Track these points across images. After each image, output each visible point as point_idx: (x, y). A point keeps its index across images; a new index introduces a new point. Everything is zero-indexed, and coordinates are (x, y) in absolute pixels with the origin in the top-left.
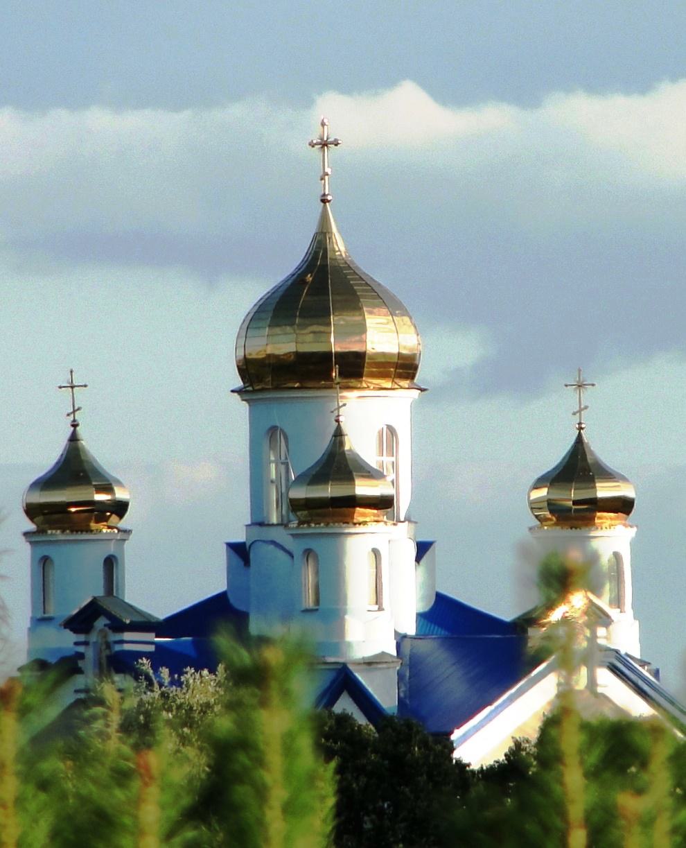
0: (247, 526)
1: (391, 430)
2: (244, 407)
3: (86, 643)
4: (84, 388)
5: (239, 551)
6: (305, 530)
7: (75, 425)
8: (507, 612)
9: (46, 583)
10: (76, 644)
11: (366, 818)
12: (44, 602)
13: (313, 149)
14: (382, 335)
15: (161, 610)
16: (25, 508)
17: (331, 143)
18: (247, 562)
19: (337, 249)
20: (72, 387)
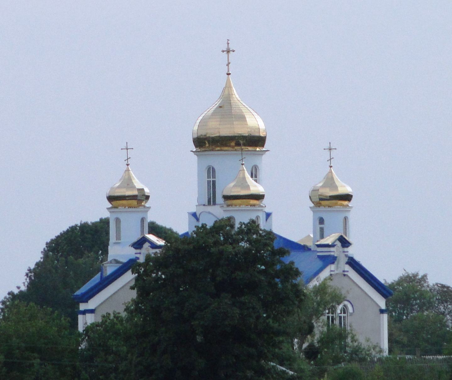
0: (196, 206)
2: (195, 157)
3: (140, 253)
4: (132, 149)
8: (338, 241)
9: (345, 223)
10: (136, 253)
11: (399, 305)
13: (223, 53)
16: (226, 199)
17: (231, 51)
19: (233, 94)
20: (127, 149)
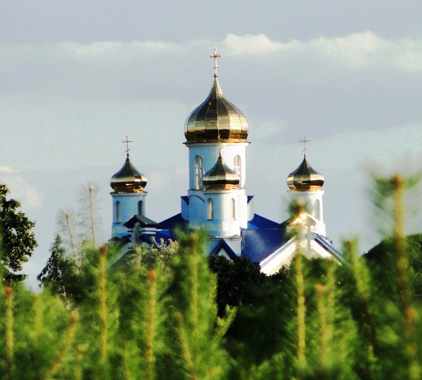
1: (239, 157)
15: (158, 220)
18: (188, 203)
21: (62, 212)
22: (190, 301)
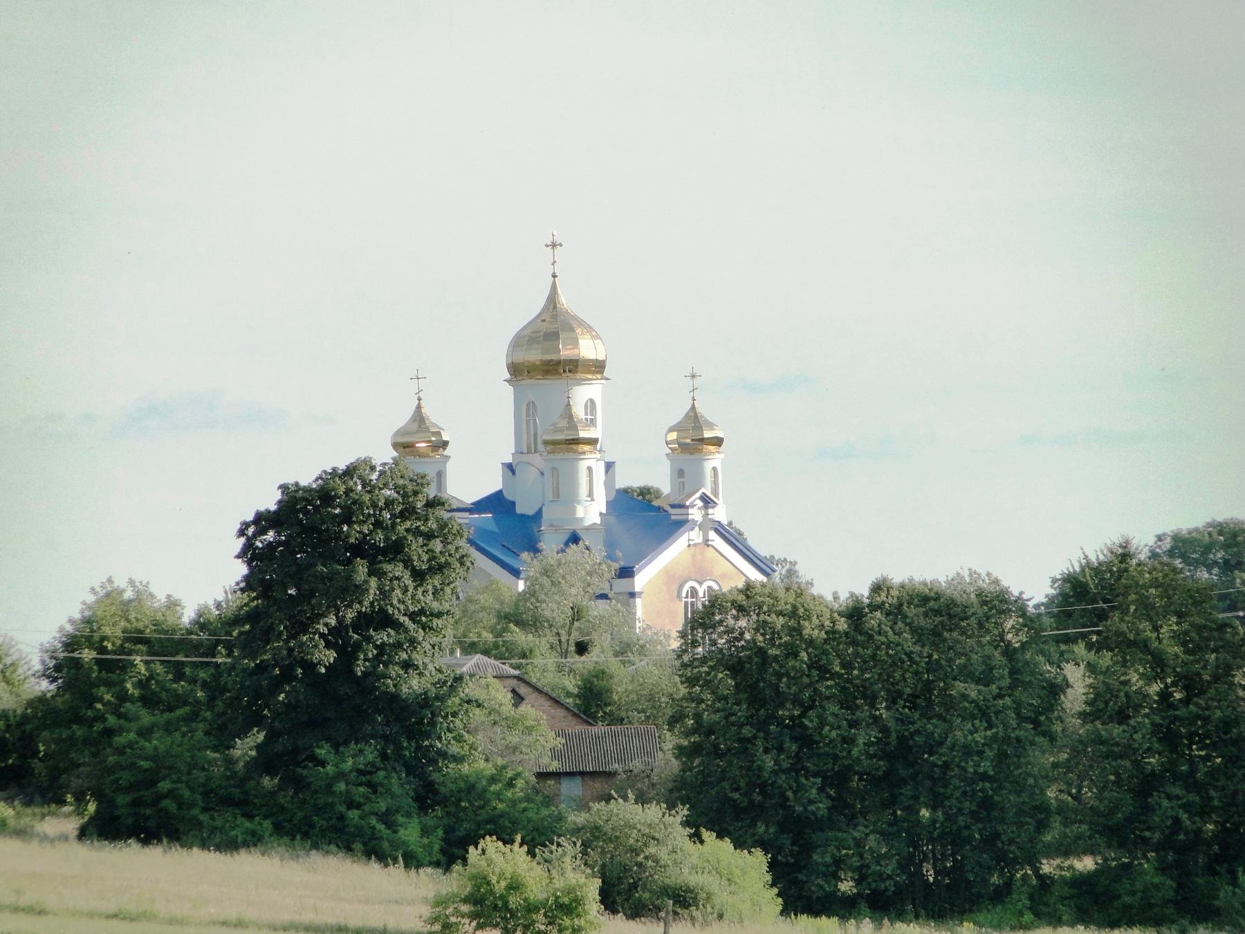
1: (592, 401)
5: (510, 468)
6: (552, 456)
7: (419, 399)
12: (582, 774)
14: (587, 349)
15: (470, 498)
18: (513, 472)
21: (1125, 545)
22: (981, 917)
